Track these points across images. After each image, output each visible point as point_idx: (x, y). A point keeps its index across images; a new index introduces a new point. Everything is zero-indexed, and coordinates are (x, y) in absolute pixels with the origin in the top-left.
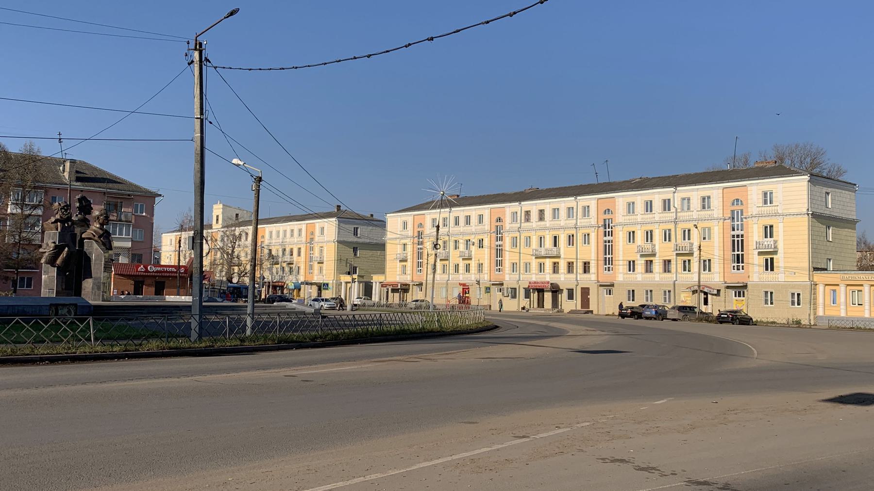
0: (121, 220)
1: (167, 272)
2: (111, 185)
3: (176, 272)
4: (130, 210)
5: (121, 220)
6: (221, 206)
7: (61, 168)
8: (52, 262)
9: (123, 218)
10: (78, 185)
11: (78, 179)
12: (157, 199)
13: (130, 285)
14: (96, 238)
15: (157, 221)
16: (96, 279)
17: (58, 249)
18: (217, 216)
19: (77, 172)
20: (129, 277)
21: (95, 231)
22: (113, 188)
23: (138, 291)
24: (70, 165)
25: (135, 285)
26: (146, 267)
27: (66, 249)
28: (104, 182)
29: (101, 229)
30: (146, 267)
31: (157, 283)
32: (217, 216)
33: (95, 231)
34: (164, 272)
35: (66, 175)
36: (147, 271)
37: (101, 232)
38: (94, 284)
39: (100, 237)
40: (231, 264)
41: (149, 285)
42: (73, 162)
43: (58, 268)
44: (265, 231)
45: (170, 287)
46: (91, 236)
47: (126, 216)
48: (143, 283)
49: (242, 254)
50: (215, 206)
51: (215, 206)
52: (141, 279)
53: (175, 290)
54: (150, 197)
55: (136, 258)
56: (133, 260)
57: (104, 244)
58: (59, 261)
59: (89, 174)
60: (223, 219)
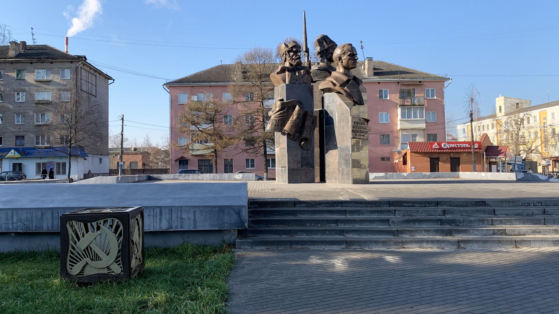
0: (414, 105)
1: (460, 148)
2: (403, 75)
3: (470, 148)
4: (422, 95)
5: (414, 105)
6: (503, 98)
7: (362, 67)
8: (280, 126)
9: (416, 103)
10: (377, 79)
11: (376, 74)
12: (446, 83)
13: (426, 162)
14: (337, 88)
15: (448, 102)
16: (342, 150)
17: (286, 108)
18: (500, 107)
19: (375, 69)
20: (424, 154)
21: (336, 79)
22: (407, 78)
23: (434, 168)
24: (369, 63)
25: (430, 162)
26: (439, 144)
27: (297, 108)
28: (397, 74)
29: (345, 74)
30: (439, 144)
31: (451, 158)
32: (500, 107)
33: (336, 79)
34: (458, 148)
35: (366, 71)
36: (441, 148)
37: (345, 78)
38: (340, 157)
39: (342, 86)
40: (517, 144)
41: (444, 162)
42: (370, 59)
43: (289, 135)
44: (546, 113)
45: (466, 163)
46: (331, 86)
47: (418, 101)
48: (438, 159)
49: (526, 134)
50: (497, 99)
51: (497, 99)
52: (435, 156)
53: (471, 166)
54: (441, 81)
55: (432, 137)
56: (429, 139)
57: (349, 95)
58: (287, 127)
59: (385, 69)
60: (505, 108)
